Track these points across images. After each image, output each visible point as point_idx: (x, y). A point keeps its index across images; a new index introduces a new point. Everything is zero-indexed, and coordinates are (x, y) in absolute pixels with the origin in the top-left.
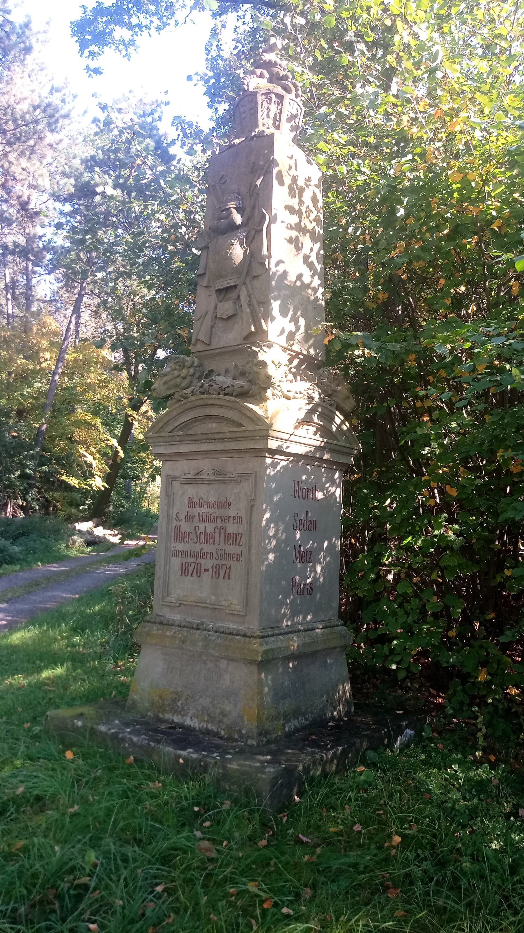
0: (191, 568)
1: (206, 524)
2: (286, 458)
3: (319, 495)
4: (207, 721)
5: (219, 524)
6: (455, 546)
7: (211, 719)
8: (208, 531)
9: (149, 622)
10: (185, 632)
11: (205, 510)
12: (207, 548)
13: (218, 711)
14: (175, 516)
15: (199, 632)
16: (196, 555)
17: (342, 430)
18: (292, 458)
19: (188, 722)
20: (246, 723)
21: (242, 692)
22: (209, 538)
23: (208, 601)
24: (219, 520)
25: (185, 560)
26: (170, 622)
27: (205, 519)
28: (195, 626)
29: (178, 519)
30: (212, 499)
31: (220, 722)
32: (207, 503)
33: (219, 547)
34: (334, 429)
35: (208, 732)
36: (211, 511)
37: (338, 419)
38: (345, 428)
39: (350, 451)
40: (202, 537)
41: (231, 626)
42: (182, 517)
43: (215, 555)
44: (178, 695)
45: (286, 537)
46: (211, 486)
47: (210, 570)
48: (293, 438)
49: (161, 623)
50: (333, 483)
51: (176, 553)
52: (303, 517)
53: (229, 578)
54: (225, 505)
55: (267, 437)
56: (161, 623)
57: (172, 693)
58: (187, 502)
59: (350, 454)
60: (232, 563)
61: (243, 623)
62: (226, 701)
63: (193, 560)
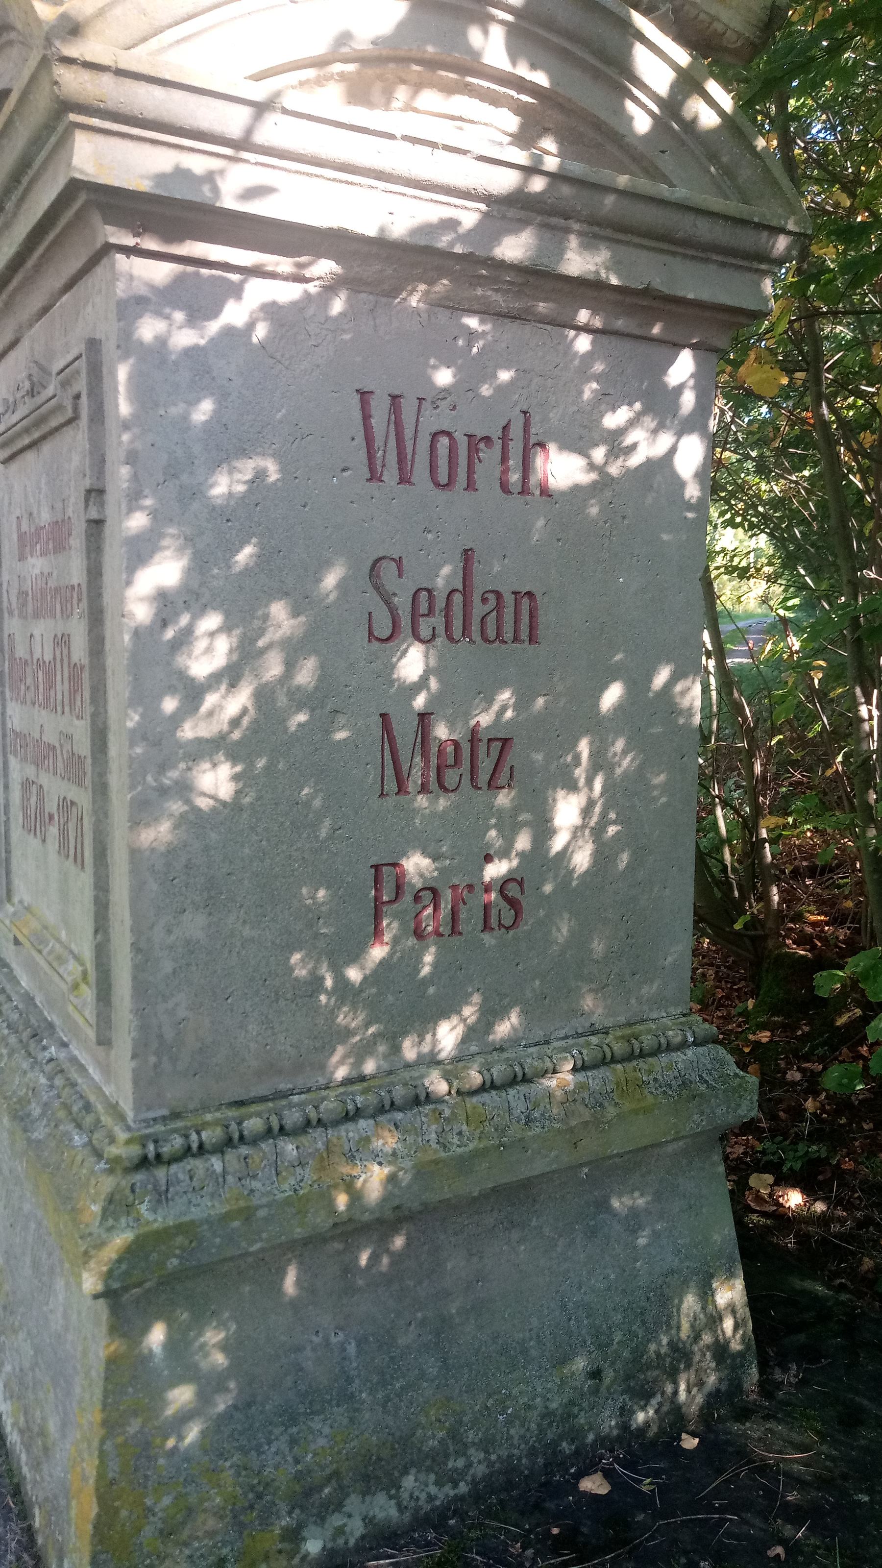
2: (284, 264)
3: (562, 469)
6: (180, 1444)
17: (690, 126)
18: (325, 267)
34: (642, 124)
37: (657, 60)
38: (708, 119)
39: (746, 239)
45: (324, 675)
48: (270, 132)
50: (660, 406)
52: (446, 575)
55: (64, 116)
59: (759, 261)
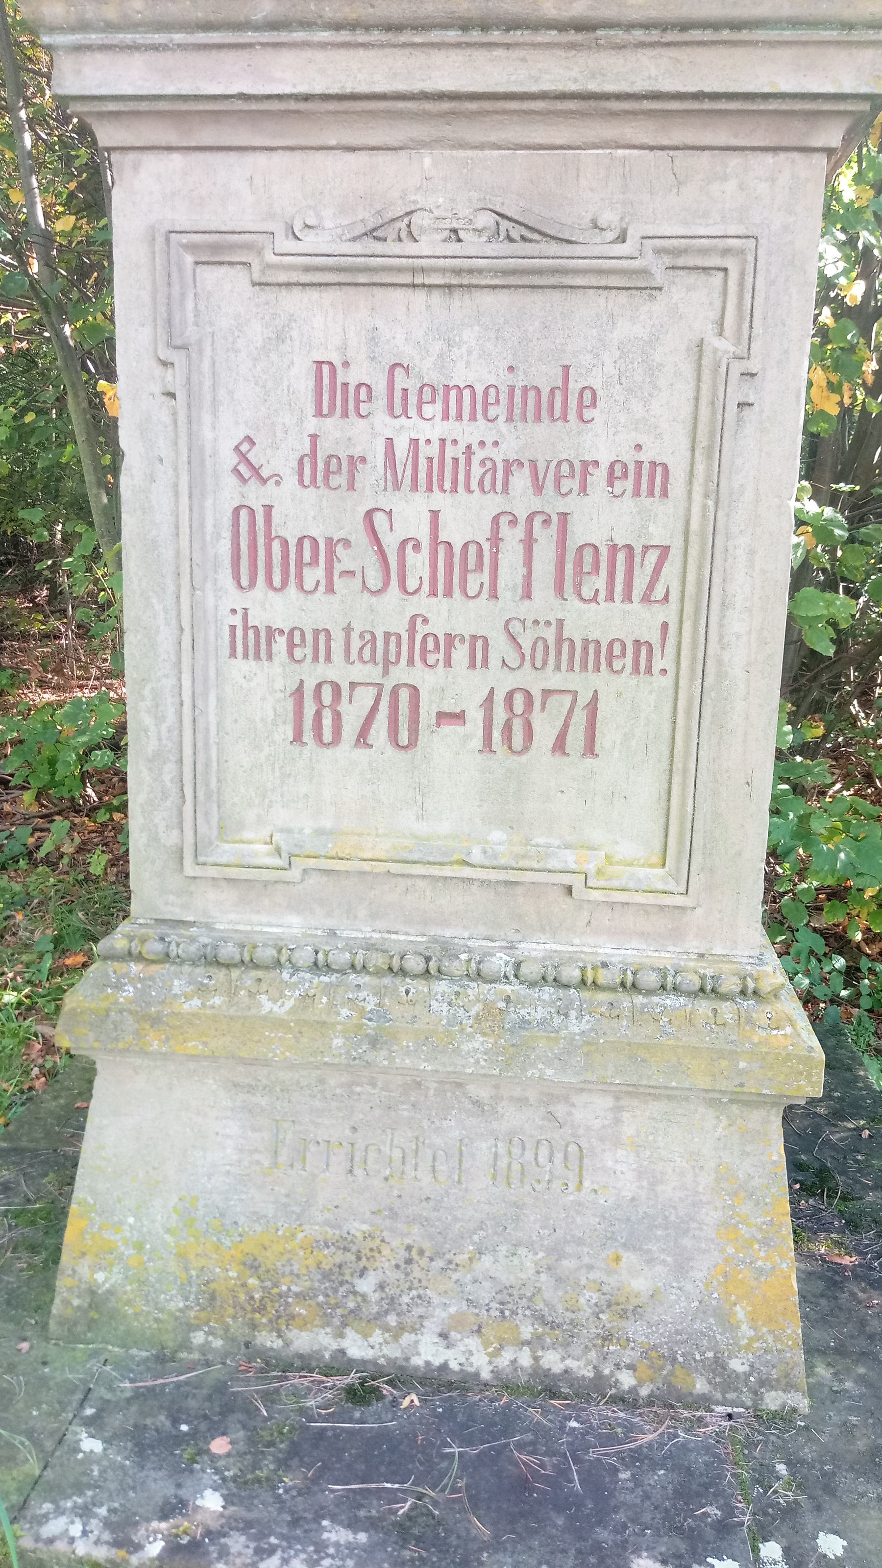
0: (353, 714)
1: (438, 500)
4: (535, 1343)
5: (522, 498)
7: (556, 1329)
8: (455, 533)
9: (129, 956)
10: (366, 992)
11: (430, 428)
12: (445, 615)
13: (588, 1298)
14: (230, 459)
15: (442, 987)
16: (381, 649)
19: (428, 1352)
20: (745, 1330)
21: (711, 1216)
22: (456, 568)
23: (476, 856)
24: (521, 480)
25: (312, 675)
26: (266, 954)
27: (438, 472)
28: (414, 964)
29: (249, 470)
30: (474, 371)
31: (607, 1338)
32: (429, 392)
33: (526, 610)
35: (548, 1387)
36: (469, 432)
40: (418, 564)
41: (606, 949)
42: (280, 459)
43: (500, 646)
44: (358, 1255)
46: (461, 304)
47: (475, 716)
49: (211, 960)
51: (255, 641)
53: (590, 749)
54: (561, 401)
56: (211, 960)
57: (313, 1246)
58: (305, 385)
60: (601, 681)
61: (676, 934)
62: (628, 1257)
63: (373, 673)
